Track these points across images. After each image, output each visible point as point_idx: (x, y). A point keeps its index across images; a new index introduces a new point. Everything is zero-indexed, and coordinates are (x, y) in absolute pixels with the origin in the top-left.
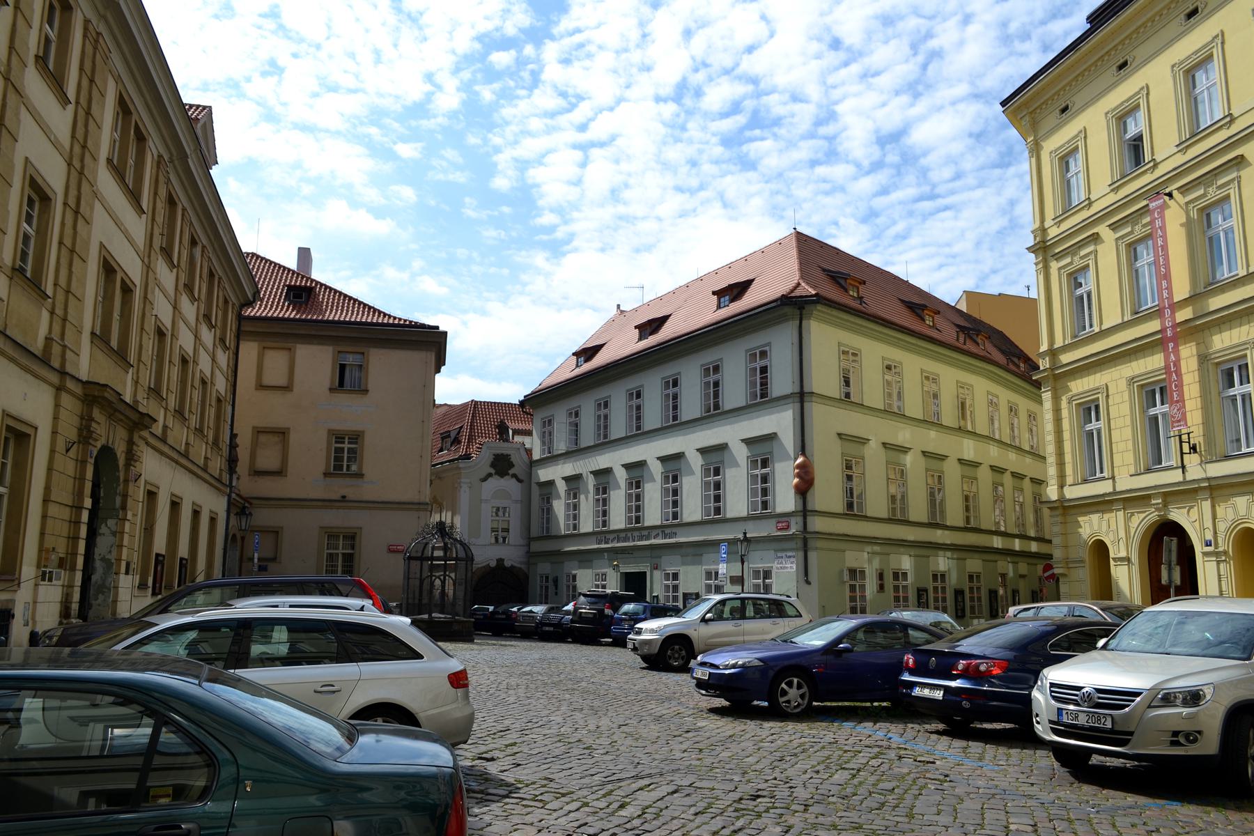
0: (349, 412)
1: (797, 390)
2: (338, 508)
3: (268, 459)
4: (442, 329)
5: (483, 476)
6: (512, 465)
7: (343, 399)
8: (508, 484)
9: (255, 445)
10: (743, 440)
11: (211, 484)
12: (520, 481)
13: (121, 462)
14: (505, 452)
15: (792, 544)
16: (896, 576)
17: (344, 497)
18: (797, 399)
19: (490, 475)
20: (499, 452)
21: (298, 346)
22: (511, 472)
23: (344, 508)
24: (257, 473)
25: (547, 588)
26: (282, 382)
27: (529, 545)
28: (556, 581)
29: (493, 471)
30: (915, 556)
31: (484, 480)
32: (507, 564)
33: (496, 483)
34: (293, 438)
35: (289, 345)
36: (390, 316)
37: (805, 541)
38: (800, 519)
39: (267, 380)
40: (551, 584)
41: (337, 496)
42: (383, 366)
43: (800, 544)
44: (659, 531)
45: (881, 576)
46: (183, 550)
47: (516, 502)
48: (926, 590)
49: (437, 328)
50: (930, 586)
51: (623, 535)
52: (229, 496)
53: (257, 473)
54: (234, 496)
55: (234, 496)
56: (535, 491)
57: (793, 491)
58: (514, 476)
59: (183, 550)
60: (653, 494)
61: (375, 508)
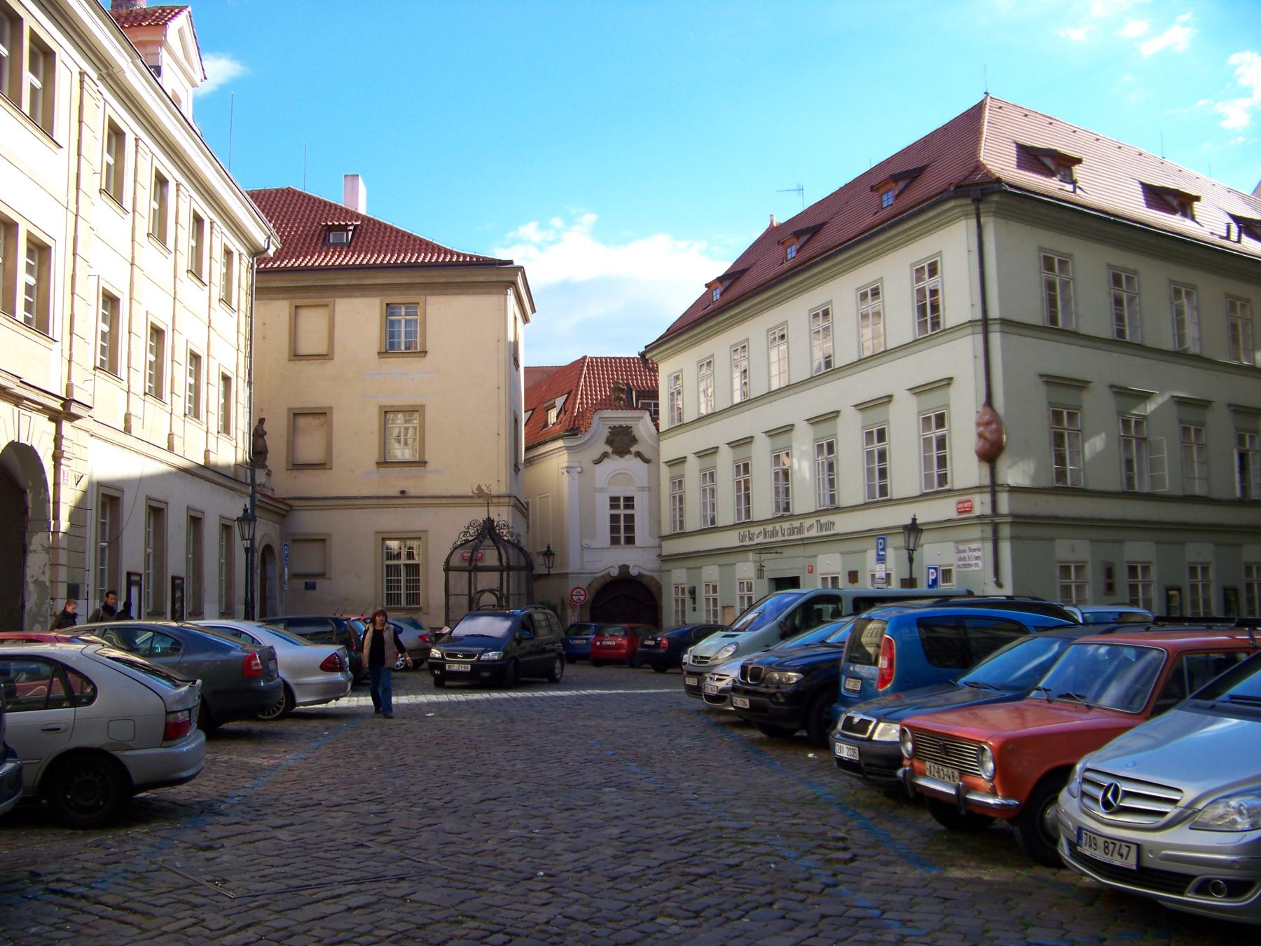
0: (404, 380)
1: (979, 316)
2: (396, 506)
3: (310, 448)
4: (516, 263)
5: (597, 456)
6: (634, 440)
7: (395, 365)
8: (629, 464)
9: (293, 431)
10: (1112, 386)
11: (217, 483)
12: (647, 461)
13: (48, 464)
14: (624, 424)
15: (976, 532)
16: (1132, 570)
17: (403, 492)
18: (980, 329)
19: (605, 455)
20: (617, 424)
21: (338, 300)
22: (633, 449)
23: (403, 506)
24: (297, 467)
25: (683, 601)
26: (323, 349)
27: (660, 546)
28: (693, 592)
29: (609, 449)
30: (1092, 541)
31: (598, 462)
32: (634, 572)
33: (616, 464)
34: (337, 418)
35: (324, 301)
36: (452, 253)
37: (996, 528)
38: (987, 498)
39: (304, 349)
40: (687, 596)
41: (395, 492)
42: (446, 316)
43: (988, 531)
44: (813, 521)
45: (1109, 572)
46: (176, 563)
47: (642, 489)
48: (1235, 590)
49: (511, 262)
50: (1185, 582)
51: (769, 528)
52: (252, 497)
53: (297, 467)
54: (258, 496)
55: (258, 496)
56: (665, 472)
57: (975, 458)
58: (638, 454)
59: (176, 563)
60: (803, 467)
61: (439, 505)
